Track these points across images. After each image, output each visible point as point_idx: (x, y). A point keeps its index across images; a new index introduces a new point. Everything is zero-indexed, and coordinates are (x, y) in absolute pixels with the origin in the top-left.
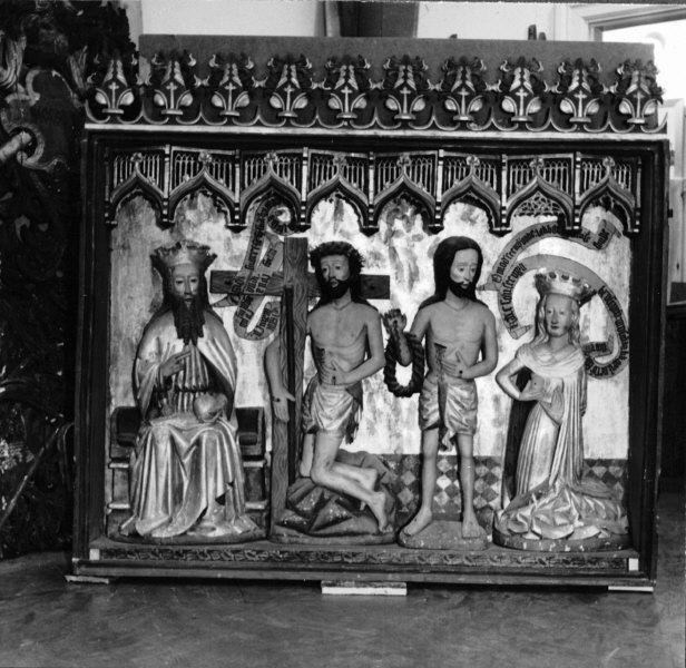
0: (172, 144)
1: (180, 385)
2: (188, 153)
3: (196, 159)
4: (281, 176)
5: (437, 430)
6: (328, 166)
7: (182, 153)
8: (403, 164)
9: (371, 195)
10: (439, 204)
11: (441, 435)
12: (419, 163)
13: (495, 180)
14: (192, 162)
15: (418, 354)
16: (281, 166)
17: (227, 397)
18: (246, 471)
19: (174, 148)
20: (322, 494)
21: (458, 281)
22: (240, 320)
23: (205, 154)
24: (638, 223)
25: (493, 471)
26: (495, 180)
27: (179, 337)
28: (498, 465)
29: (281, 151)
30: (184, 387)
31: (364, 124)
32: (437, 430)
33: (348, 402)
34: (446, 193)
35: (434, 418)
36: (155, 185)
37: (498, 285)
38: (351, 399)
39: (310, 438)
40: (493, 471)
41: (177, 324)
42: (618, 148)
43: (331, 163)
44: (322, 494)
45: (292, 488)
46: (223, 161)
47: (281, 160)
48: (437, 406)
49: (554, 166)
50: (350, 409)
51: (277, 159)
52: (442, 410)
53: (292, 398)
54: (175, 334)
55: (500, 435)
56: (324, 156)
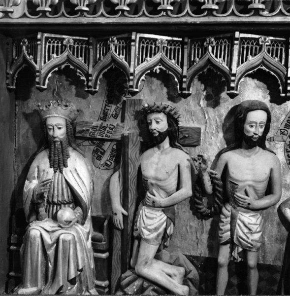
0: (43, 32)
1: (50, 200)
2: (56, 39)
3: (62, 43)
4: (119, 55)
5: (229, 245)
6: (153, 46)
7: (52, 38)
8: (209, 44)
9: (185, 68)
10: (234, 75)
11: (232, 250)
12: (221, 43)
13: (284, 56)
14: (60, 45)
15: (217, 187)
16: (119, 47)
17: (82, 209)
18: (96, 260)
19: (46, 35)
20: (143, 284)
21: (251, 134)
22: (96, 156)
23: (68, 39)
24: (289, 88)
25: (274, 276)
26: (284, 56)
27: (51, 167)
28: (278, 271)
29: (120, 36)
30: (52, 201)
31: (36, 16)
32: (229, 245)
33: (163, 221)
34: (242, 66)
35: (227, 235)
36: (224, 65)
37: (285, 137)
38: (166, 217)
39: (136, 242)
40: (274, 276)
41: (50, 158)
42: (15, 28)
43: (155, 45)
44: (143, 284)
45: (123, 275)
46: (82, 44)
47: (120, 43)
48: (228, 226)
49: (175, 45)
50: (165, 224)
51: (116, 42)
52: (232, 230)
53: (125, 213)
54: (48, 165)
55: (280, 250)
56: (150, 39)
